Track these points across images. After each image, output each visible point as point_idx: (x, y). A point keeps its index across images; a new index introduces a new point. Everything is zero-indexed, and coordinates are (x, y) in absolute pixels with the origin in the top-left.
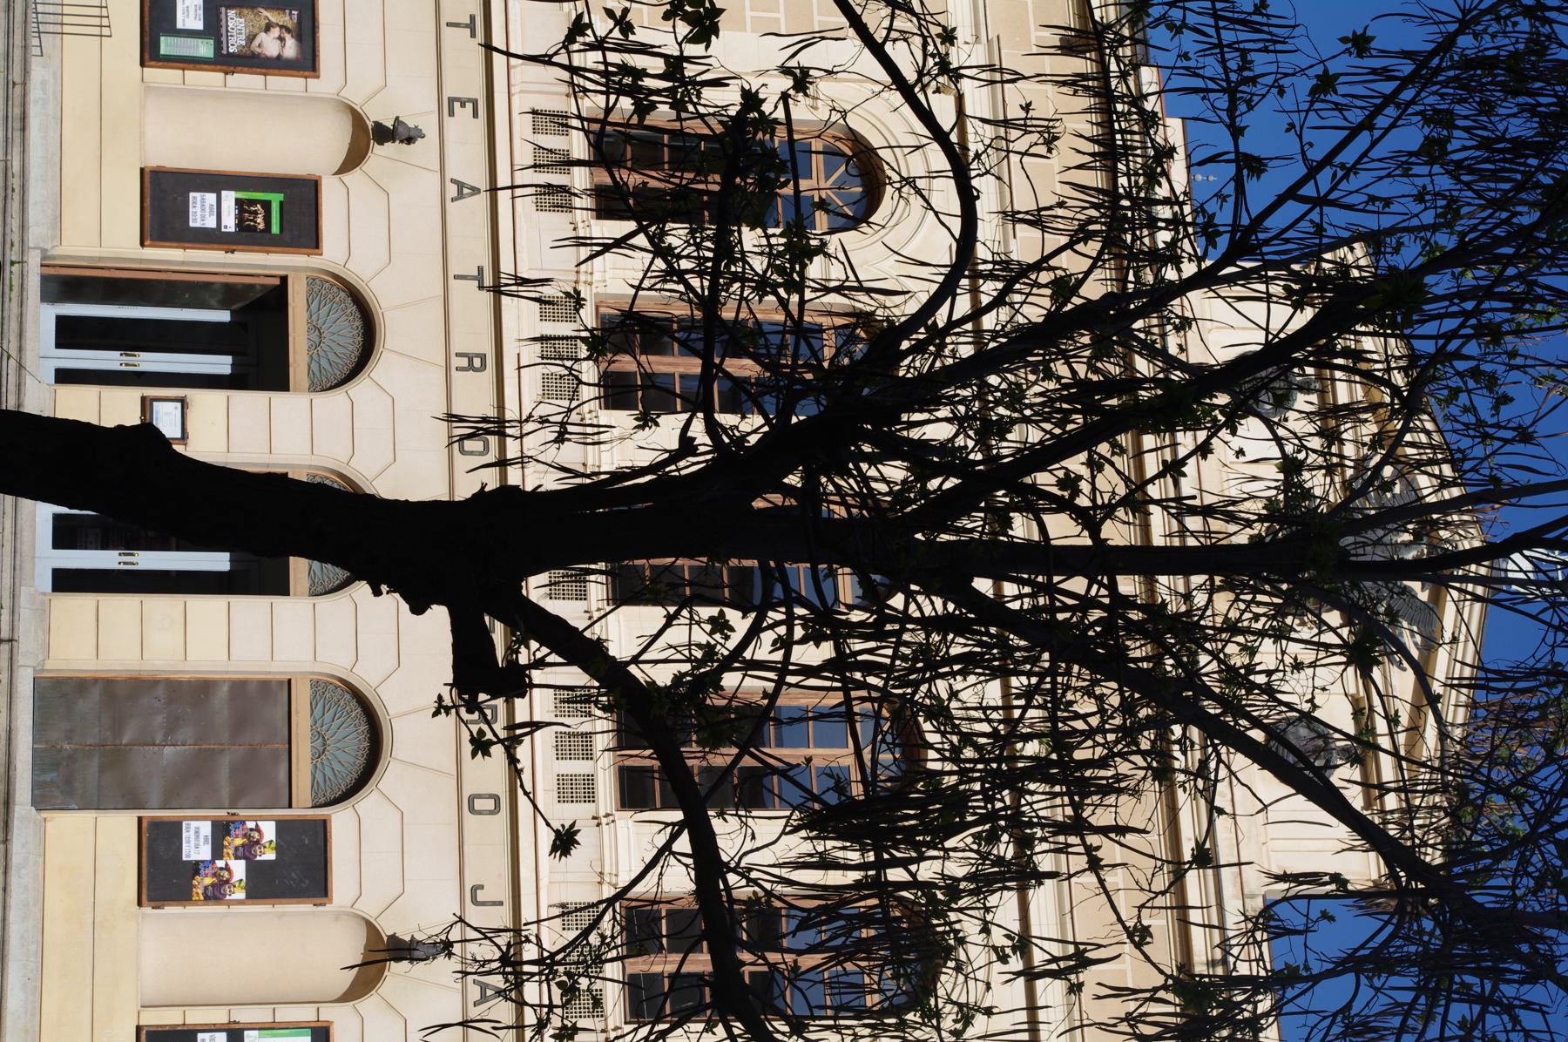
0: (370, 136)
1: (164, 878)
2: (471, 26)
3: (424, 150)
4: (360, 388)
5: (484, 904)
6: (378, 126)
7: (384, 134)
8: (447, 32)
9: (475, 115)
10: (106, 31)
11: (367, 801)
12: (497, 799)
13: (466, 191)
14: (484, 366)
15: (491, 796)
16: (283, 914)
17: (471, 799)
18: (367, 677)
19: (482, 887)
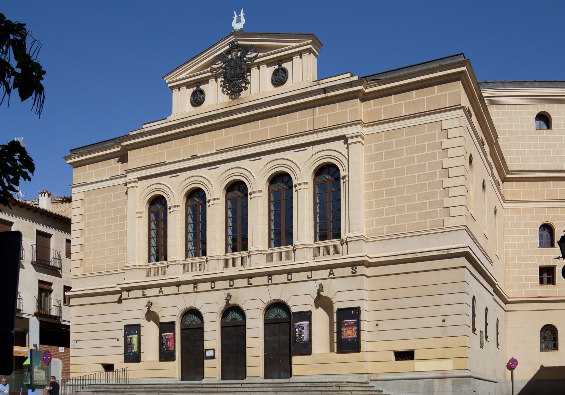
11: (290, 304)
18: (262, 306)
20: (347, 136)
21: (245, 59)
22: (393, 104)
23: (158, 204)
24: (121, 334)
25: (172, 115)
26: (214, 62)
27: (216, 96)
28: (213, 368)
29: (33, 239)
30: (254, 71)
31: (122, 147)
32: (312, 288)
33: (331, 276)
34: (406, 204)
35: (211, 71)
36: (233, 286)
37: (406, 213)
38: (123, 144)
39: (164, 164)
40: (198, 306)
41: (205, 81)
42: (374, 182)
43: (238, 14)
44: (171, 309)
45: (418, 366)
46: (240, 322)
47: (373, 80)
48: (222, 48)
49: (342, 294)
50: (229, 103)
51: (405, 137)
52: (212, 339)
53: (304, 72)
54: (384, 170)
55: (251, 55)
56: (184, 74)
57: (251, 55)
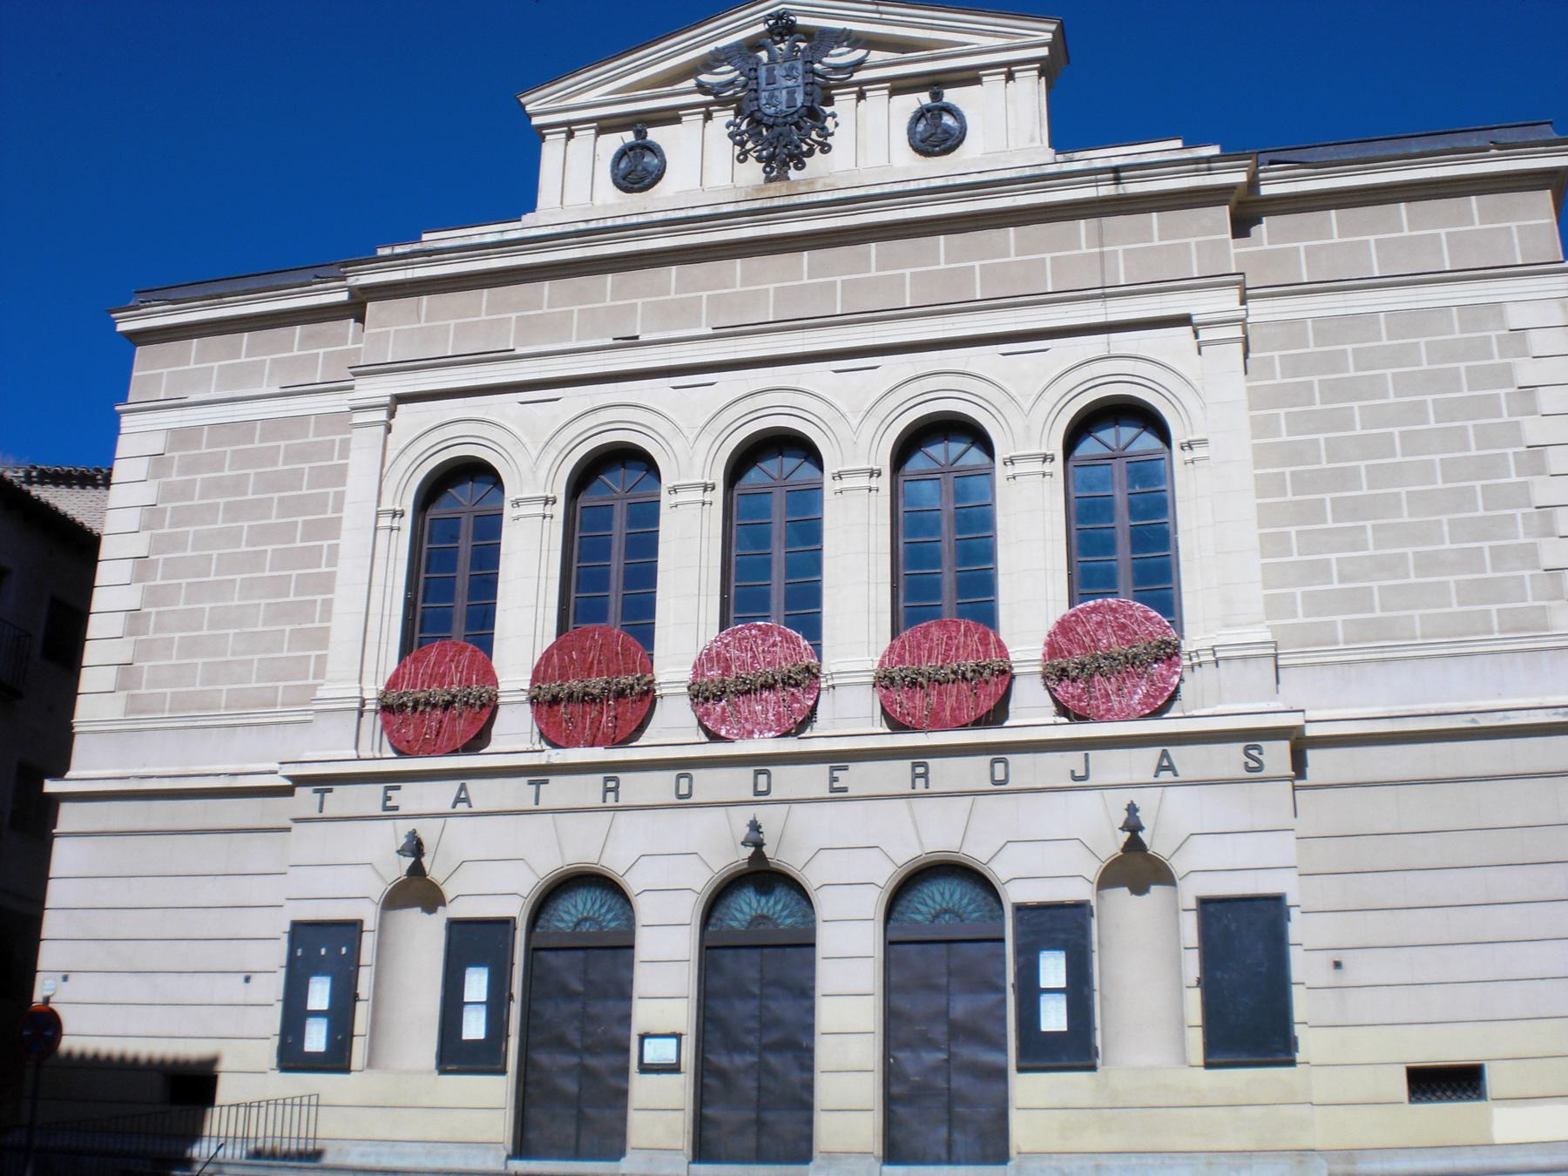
1: (1074, 1050)
2: (538, 784)
3: (428, 831)
4: (632, 884)
5: (1007, 775)
8: (327, 813)
10: (314, 1101)
11: (998, 872)
13: (1165, 763)
16: (1099, 943)
17: (995, 783)
18: (885, 874)
20: (1195, 319)
21: (817, 66)
23: (458, 494)
24: (278, 953)
25: (538, 212)
27: (704, 164)
28: (659, 1110)
30: (843, 104)
31: (351, 290)
33: (1166, 776)
34: (1410, 550)
35: (702, 88)
36: (767, 793)
38: (353, 281)
39: (508, 356)
40: (614, 863)
41: (671, 117)
42: (1288, 470)
44: (497, 863)
45: (1505, 1122)
46: (615, 932)
47: (1272, 163)
49: (1223, 840)
50: (758, 189)
52: (664, 995)
53: (1007, 124)
55: (842, 56)
57: (842, 56)
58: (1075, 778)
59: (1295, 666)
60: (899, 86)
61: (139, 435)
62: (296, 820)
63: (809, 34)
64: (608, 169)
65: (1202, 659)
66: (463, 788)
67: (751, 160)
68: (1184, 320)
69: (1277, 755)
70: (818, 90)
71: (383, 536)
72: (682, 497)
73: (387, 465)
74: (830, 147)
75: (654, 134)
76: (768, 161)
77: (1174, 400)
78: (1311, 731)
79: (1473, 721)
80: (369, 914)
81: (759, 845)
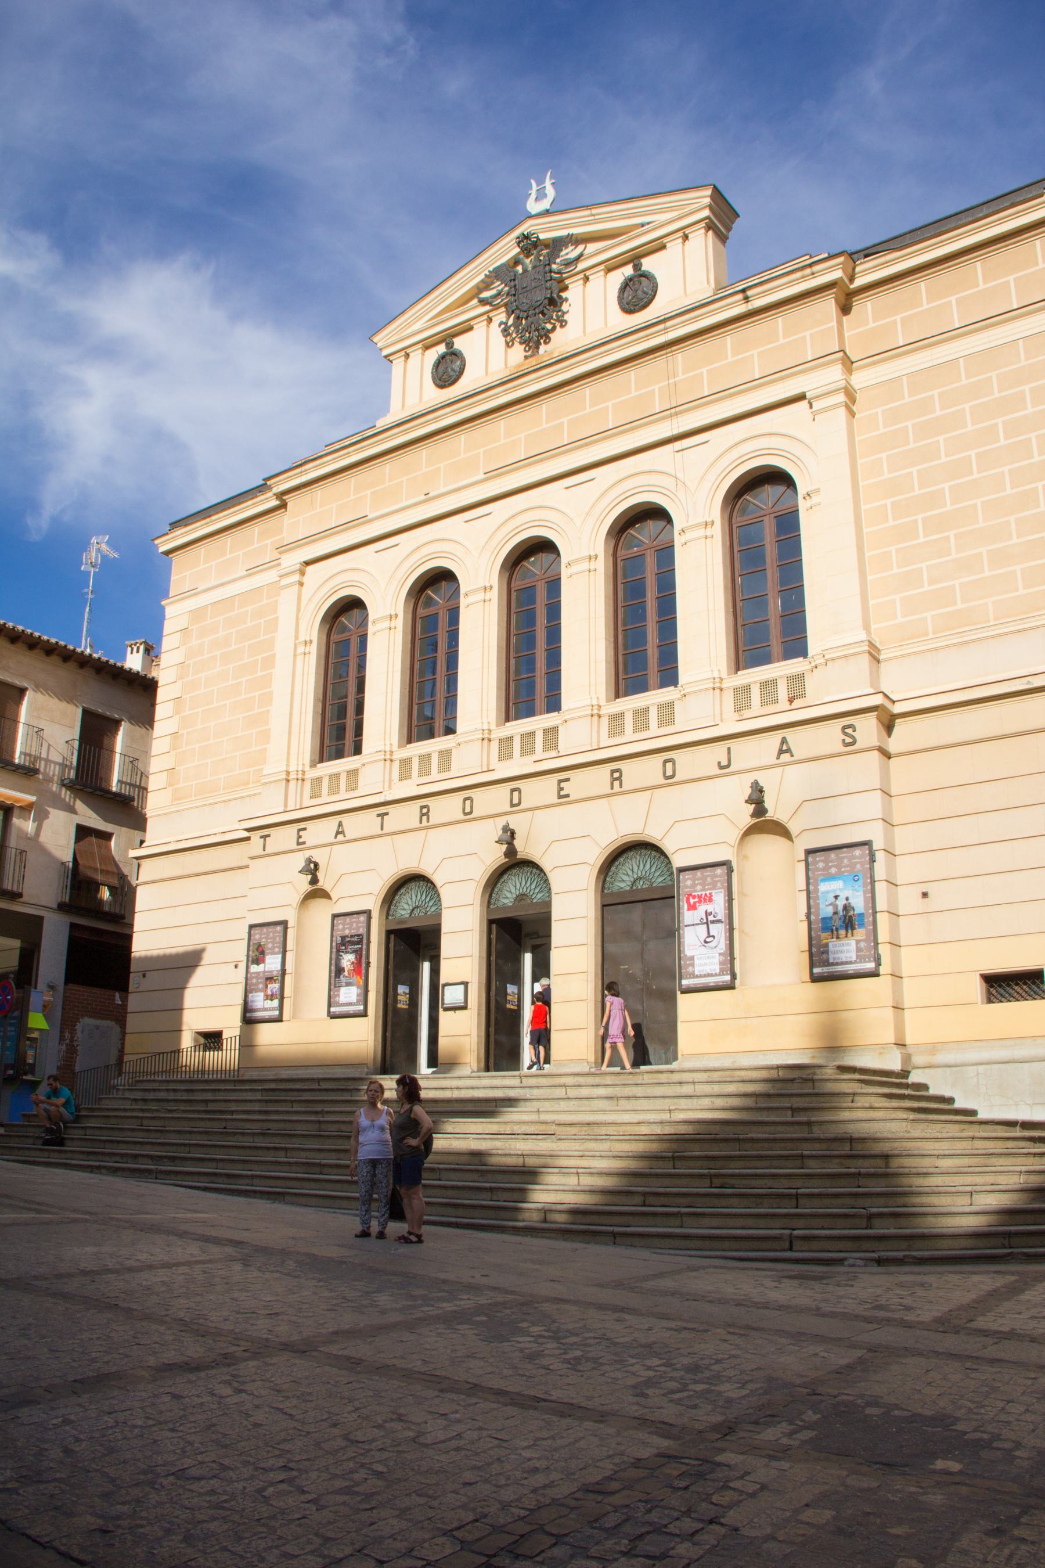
0: (763, 823)
2: (382, 815)
6: (753, 816)
7: (760, 810)
8: (268, 851)
9: (568, 780)
12: (513, 791)
13: (785, 748)
14: (618, 770)
15: (512, 794)
17: (465, 814)
18: (596, 855)
19: (719, 763)
22: (925, 306)
26: (486, 285)
27: (489, 352)
29: (72, 727)
32: (731, 801)
35: (483, 302)
37: (987, 573)
38: (275, 490)
41: (466, 328)
42: (889, 502)
43: (540, 182)
44: (360, 884)
48: (505, 250)
51: (964, 382)
53: (686, 272)
54: (914, 470)
56: (419, 321)
57: (570, 252)
58: (721, 767)
59: (894, 658)
60: (611, 267)
61: (176, 614)
62: (252, 858)
63: (546, 244)
64: (616, 295)
65: (818, 662)
66: (340, 824)
67: (516, 344)
68: (801, 397)
69: (868, 728)
70: (554, 283)
71: (300, 659)
72: (574, 569)
73: (302, 609)
74: (566, 322)
75: (648, 264)
76: (525, 342)
77: (798, 462)
78: (897, 709)
79: (1029, 683)
80: (290, 915)
81: (510, 844)
